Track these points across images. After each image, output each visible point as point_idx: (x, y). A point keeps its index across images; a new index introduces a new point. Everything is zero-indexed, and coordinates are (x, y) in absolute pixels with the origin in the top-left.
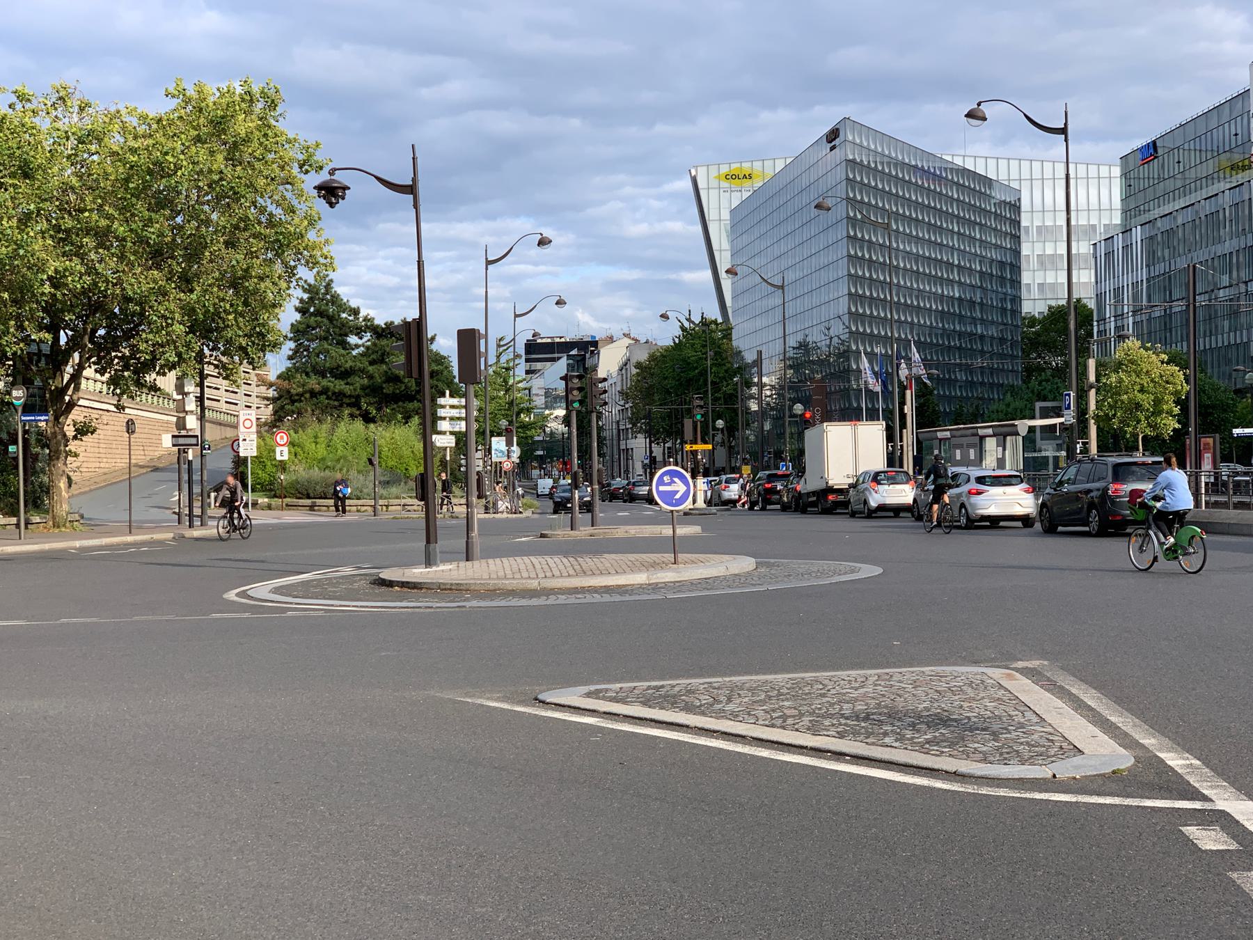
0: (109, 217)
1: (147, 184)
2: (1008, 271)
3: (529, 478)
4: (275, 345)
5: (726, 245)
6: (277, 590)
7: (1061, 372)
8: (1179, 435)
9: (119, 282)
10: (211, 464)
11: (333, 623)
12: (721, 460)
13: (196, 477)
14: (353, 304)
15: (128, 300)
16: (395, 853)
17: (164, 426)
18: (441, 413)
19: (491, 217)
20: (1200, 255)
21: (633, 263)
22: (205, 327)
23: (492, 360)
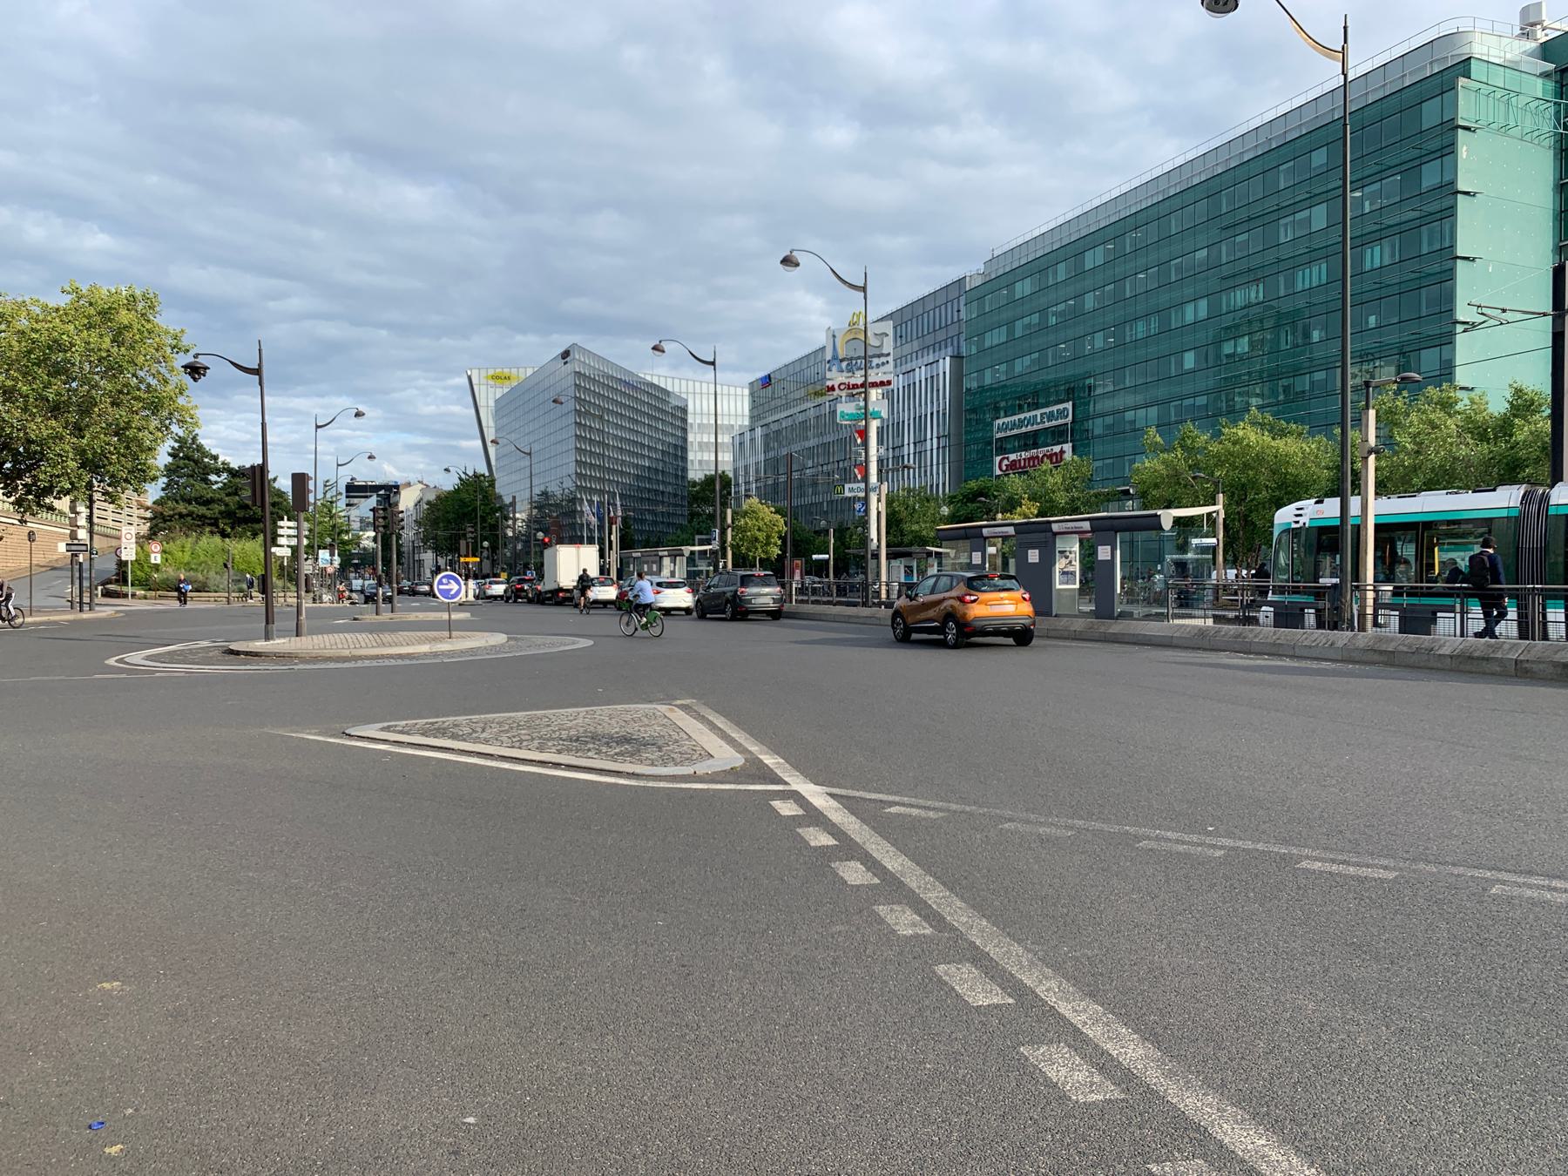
0: (15, 379)
1: (47, 356)
2: (680, 451)
3: (347, 579)
4: (154, 479)
5: (492, 424)
6: (148, 658)
7: (712, 517)
8: (781, 558)
9: (24, 428)
10: (97, 565)
11: (192, 681)
12: (486, 568)
13: (86, 575)
14: (214, 452)
15: (30, 442)
16: (231, 844)
17: (60, 537)
18: (280, 531)
19: (321, 395)
20: (796, 447)
21: (425, 432)
22: (93, 464)
23: (320, 496)
